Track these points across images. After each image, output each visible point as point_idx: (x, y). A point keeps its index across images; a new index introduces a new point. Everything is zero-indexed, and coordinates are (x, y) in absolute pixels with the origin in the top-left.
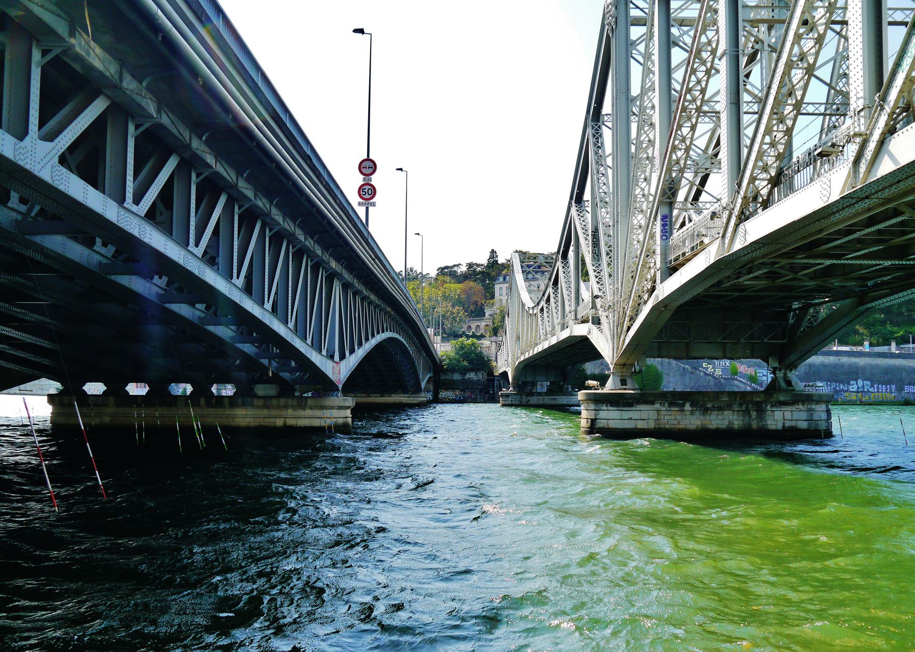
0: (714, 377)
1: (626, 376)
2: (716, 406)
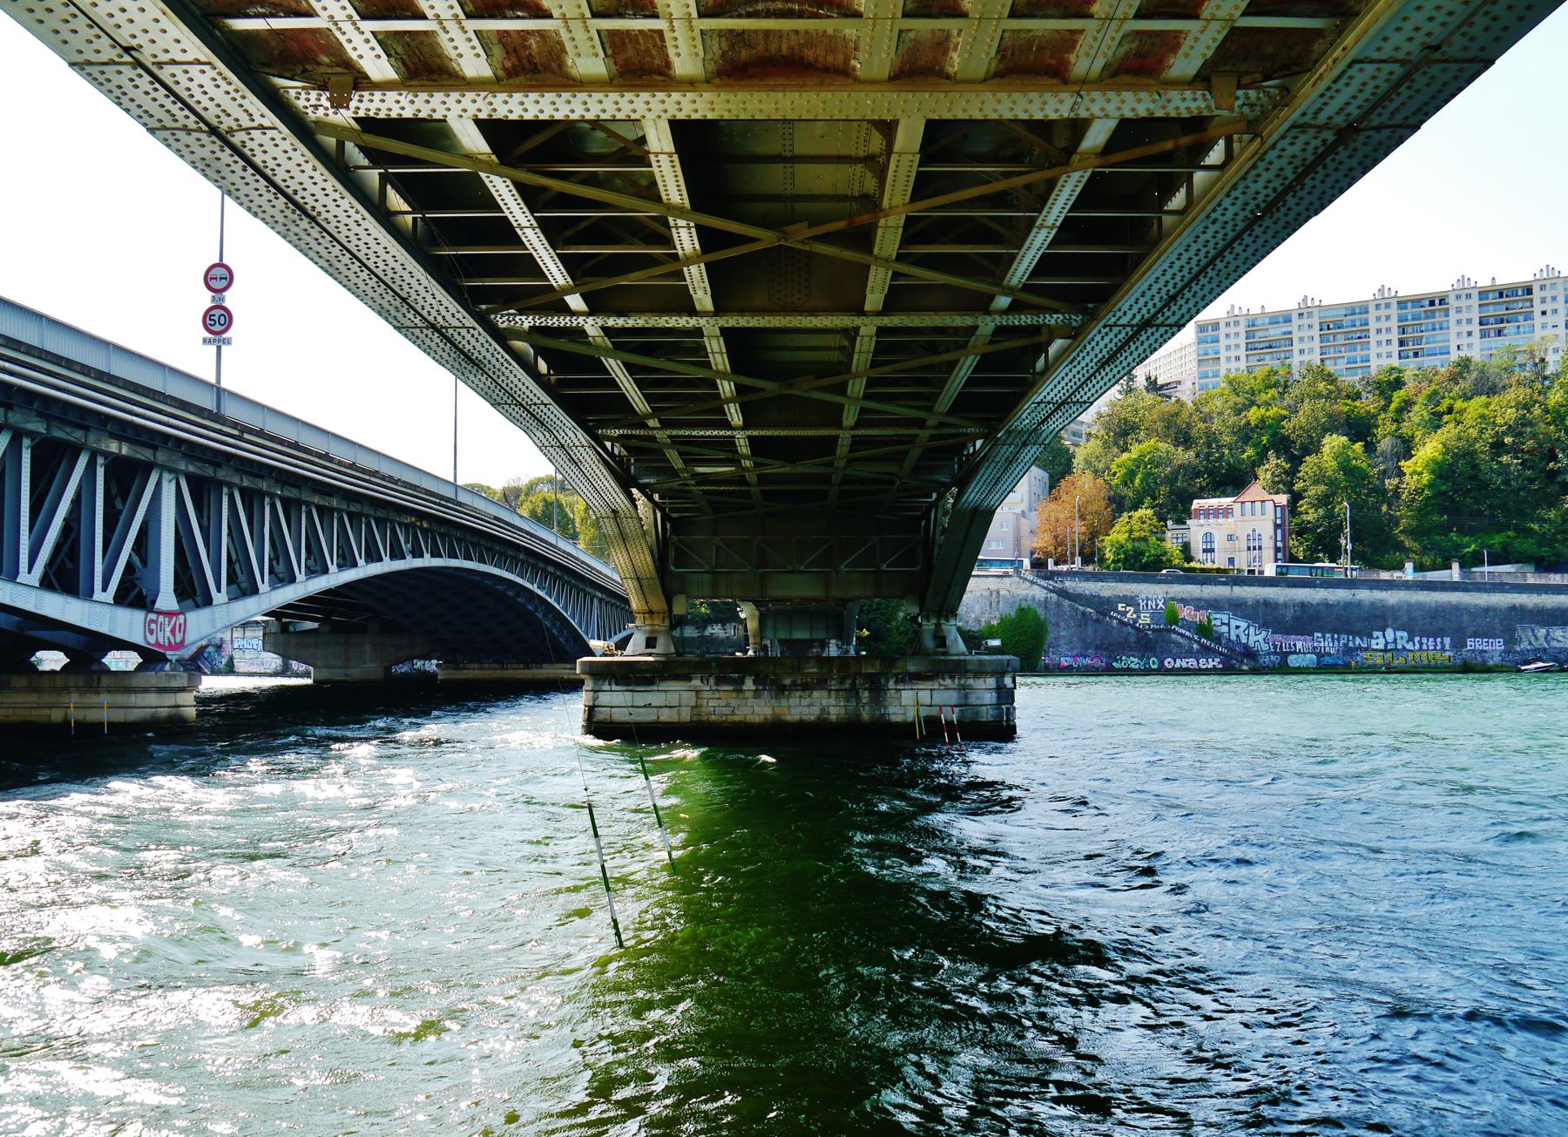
0: (1136, 628)
1: (658, 631)
2: (799, 682)
